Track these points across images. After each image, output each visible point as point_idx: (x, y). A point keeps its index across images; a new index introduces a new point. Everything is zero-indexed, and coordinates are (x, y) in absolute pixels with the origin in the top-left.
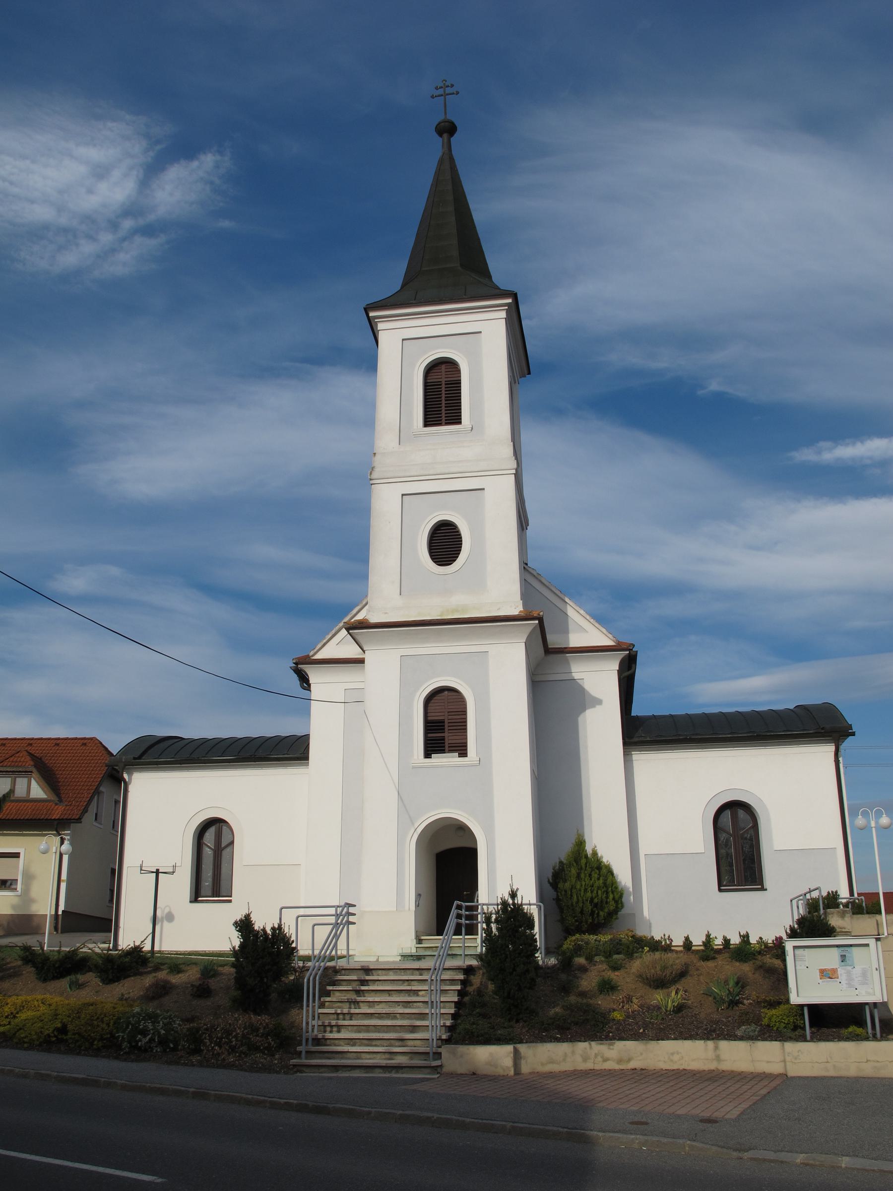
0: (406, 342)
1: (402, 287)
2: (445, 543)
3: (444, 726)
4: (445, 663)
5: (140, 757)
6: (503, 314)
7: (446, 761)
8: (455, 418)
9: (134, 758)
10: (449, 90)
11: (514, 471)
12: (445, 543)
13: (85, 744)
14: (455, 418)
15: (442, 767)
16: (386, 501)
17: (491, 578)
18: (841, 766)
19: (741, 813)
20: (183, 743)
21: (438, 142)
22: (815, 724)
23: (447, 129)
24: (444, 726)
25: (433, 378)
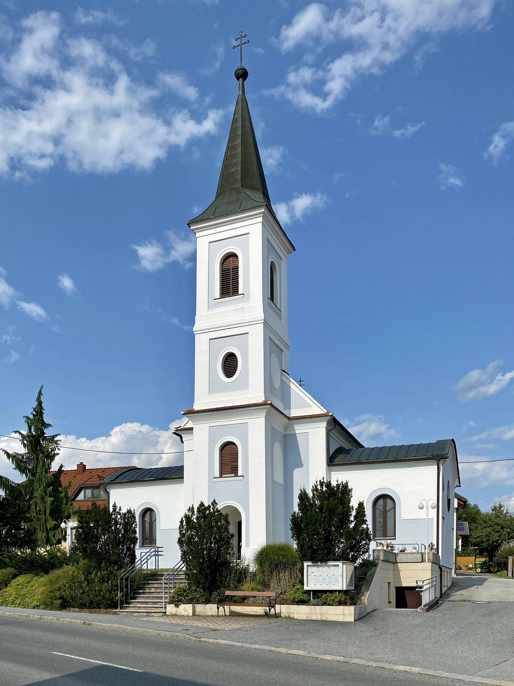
0: (209, 245)
1: (218, 195)
2: (230, 365)
3: (229, 459)
4: (228, 429)
5: (113, 481)
6: (260, 219)
7: (229, 480)
8: (235, 292)
9: (111, 481)
10: (244, 40)
11: (263, 321)
12: (230, 365)
13: (104, 472)
14: (235, 292)
15: (227, 481)
16: (201, 344)
17: (250, 385)
18: (441, 473)
19: (388, 501)
20: (176, 469)
21: (236, 83)
22: (439, 453)
23: (242, 75)
24: (229, 459)
25: (226, 266)
